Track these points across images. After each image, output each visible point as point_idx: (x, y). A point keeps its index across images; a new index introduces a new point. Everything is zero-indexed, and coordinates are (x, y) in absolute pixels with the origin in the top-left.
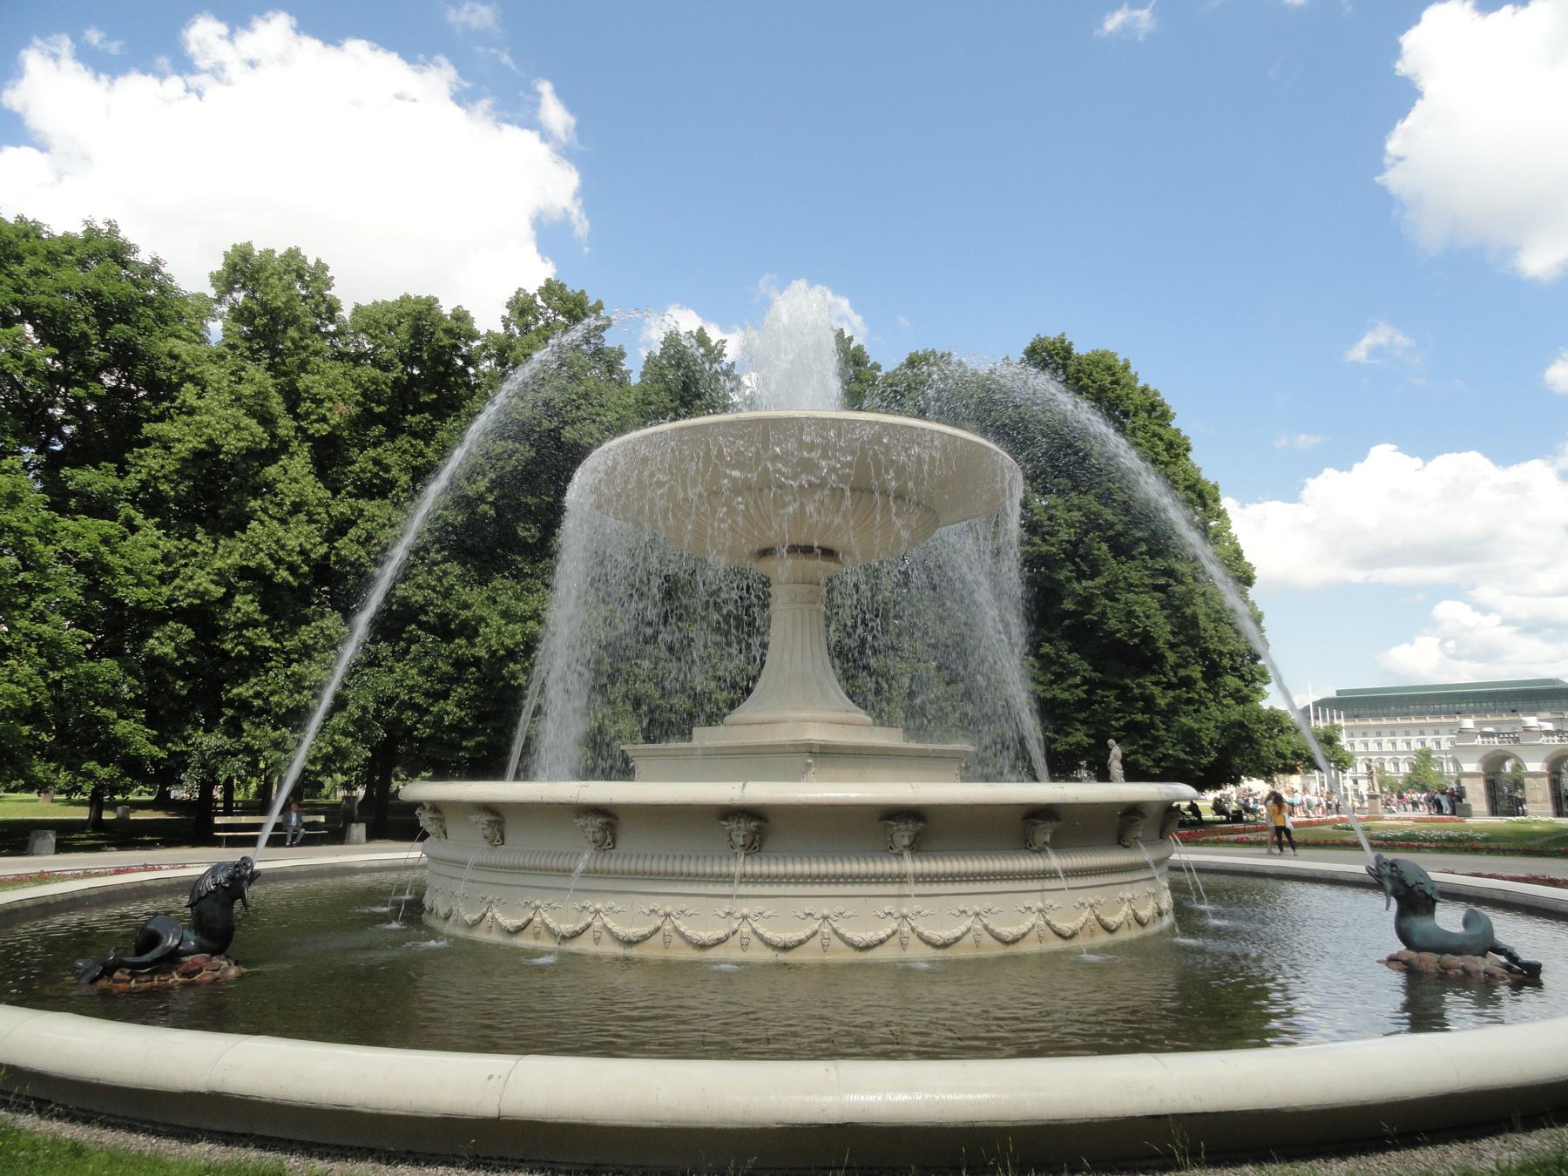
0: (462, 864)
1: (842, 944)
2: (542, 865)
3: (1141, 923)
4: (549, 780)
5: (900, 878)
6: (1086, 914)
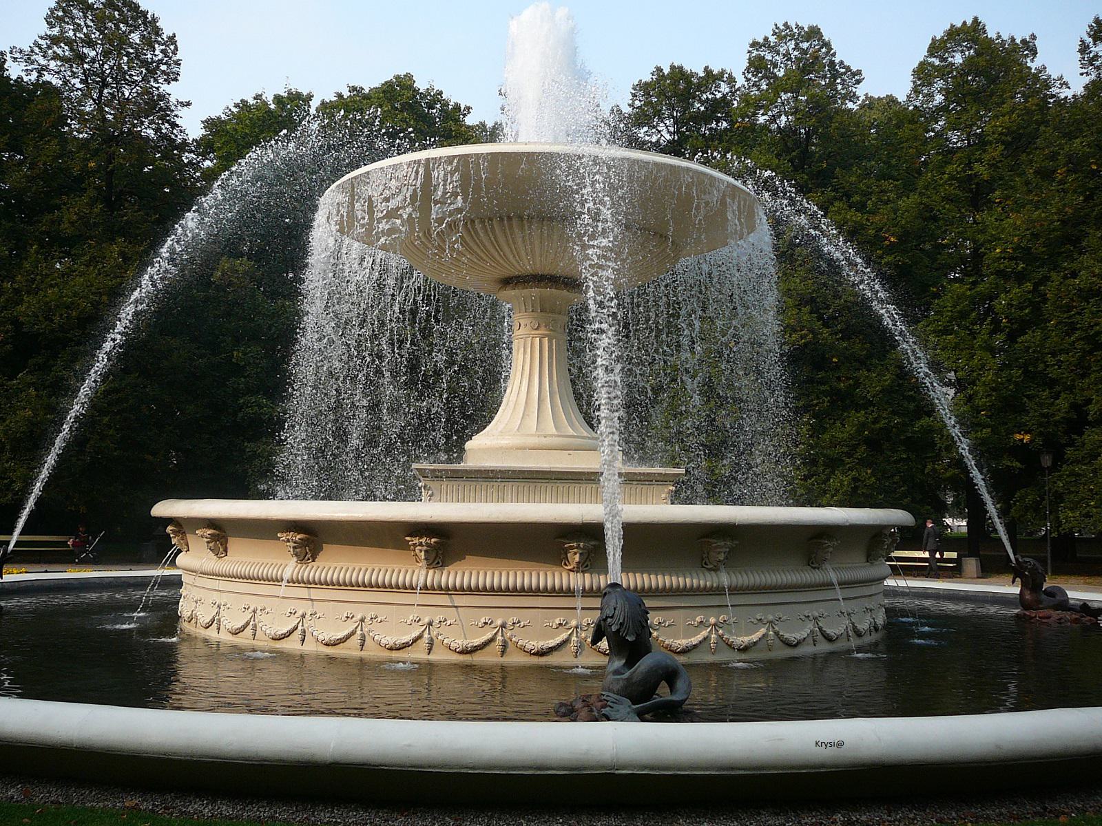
3: (859, 634)
6: (810, 626)
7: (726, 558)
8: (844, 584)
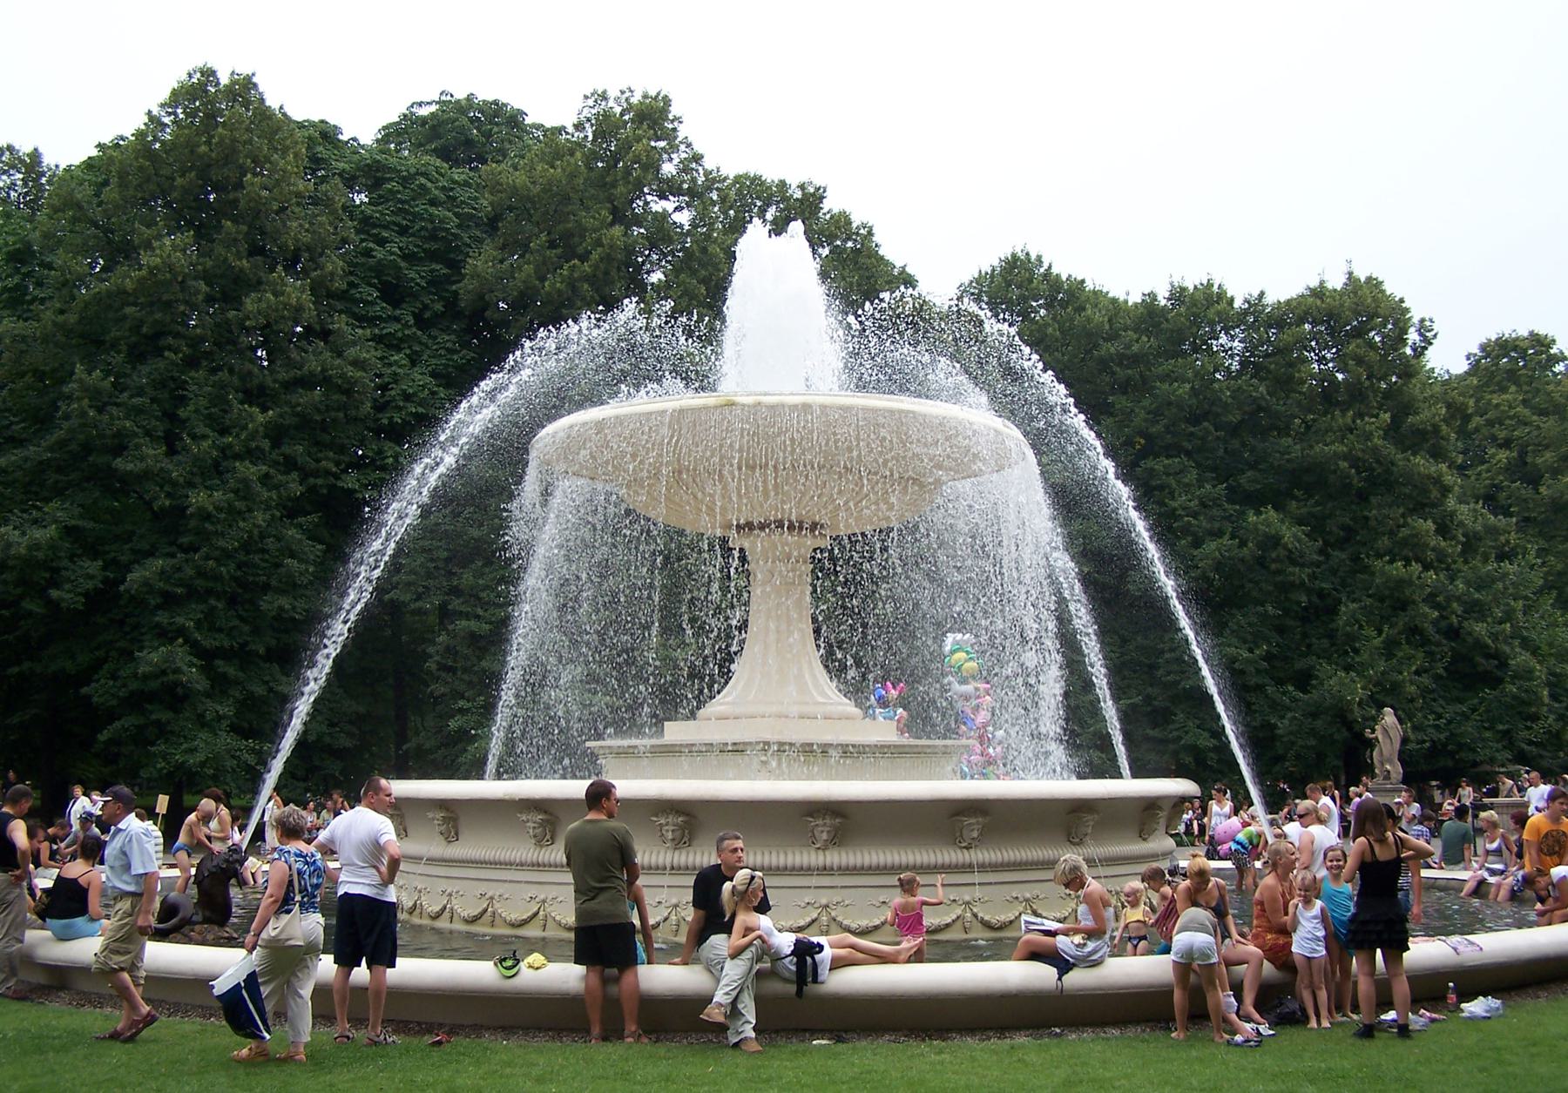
2: (546, 861)
4: (537, 777)
7: (981, 834)
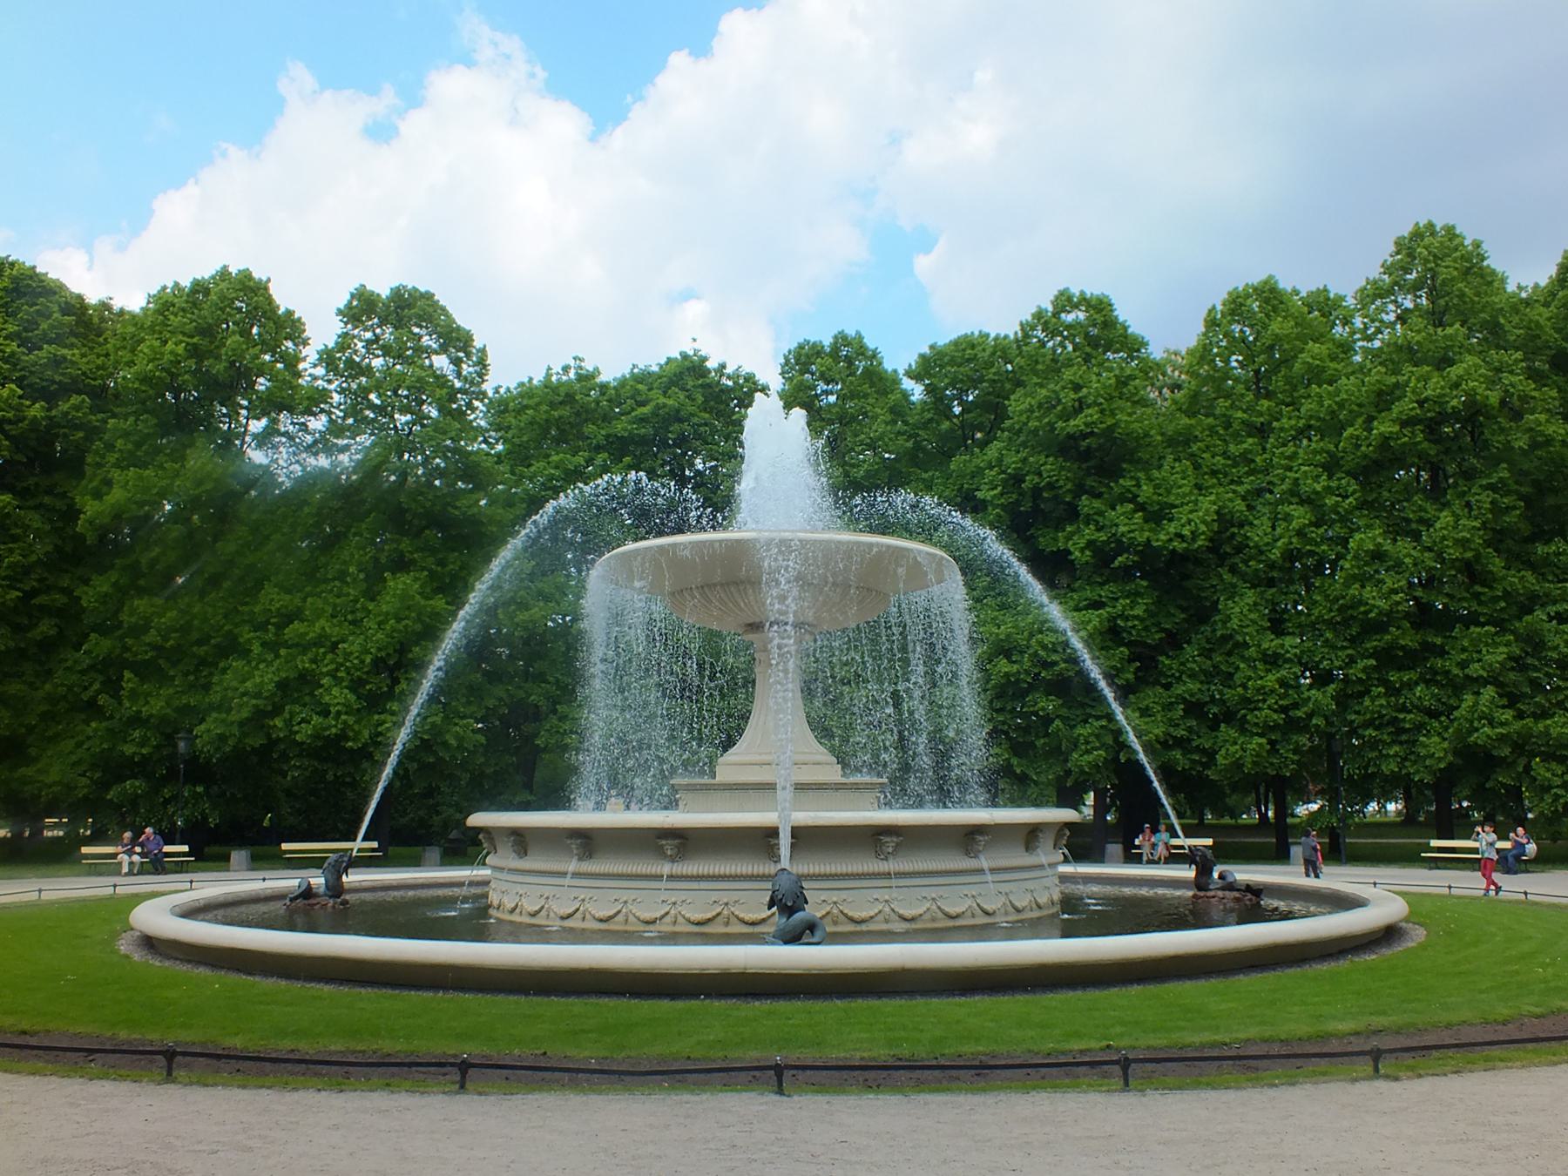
0: (563, 874)
1: (684, 921)
3: (1039, 907)
5: (659, 877)
8: (993, 870)
